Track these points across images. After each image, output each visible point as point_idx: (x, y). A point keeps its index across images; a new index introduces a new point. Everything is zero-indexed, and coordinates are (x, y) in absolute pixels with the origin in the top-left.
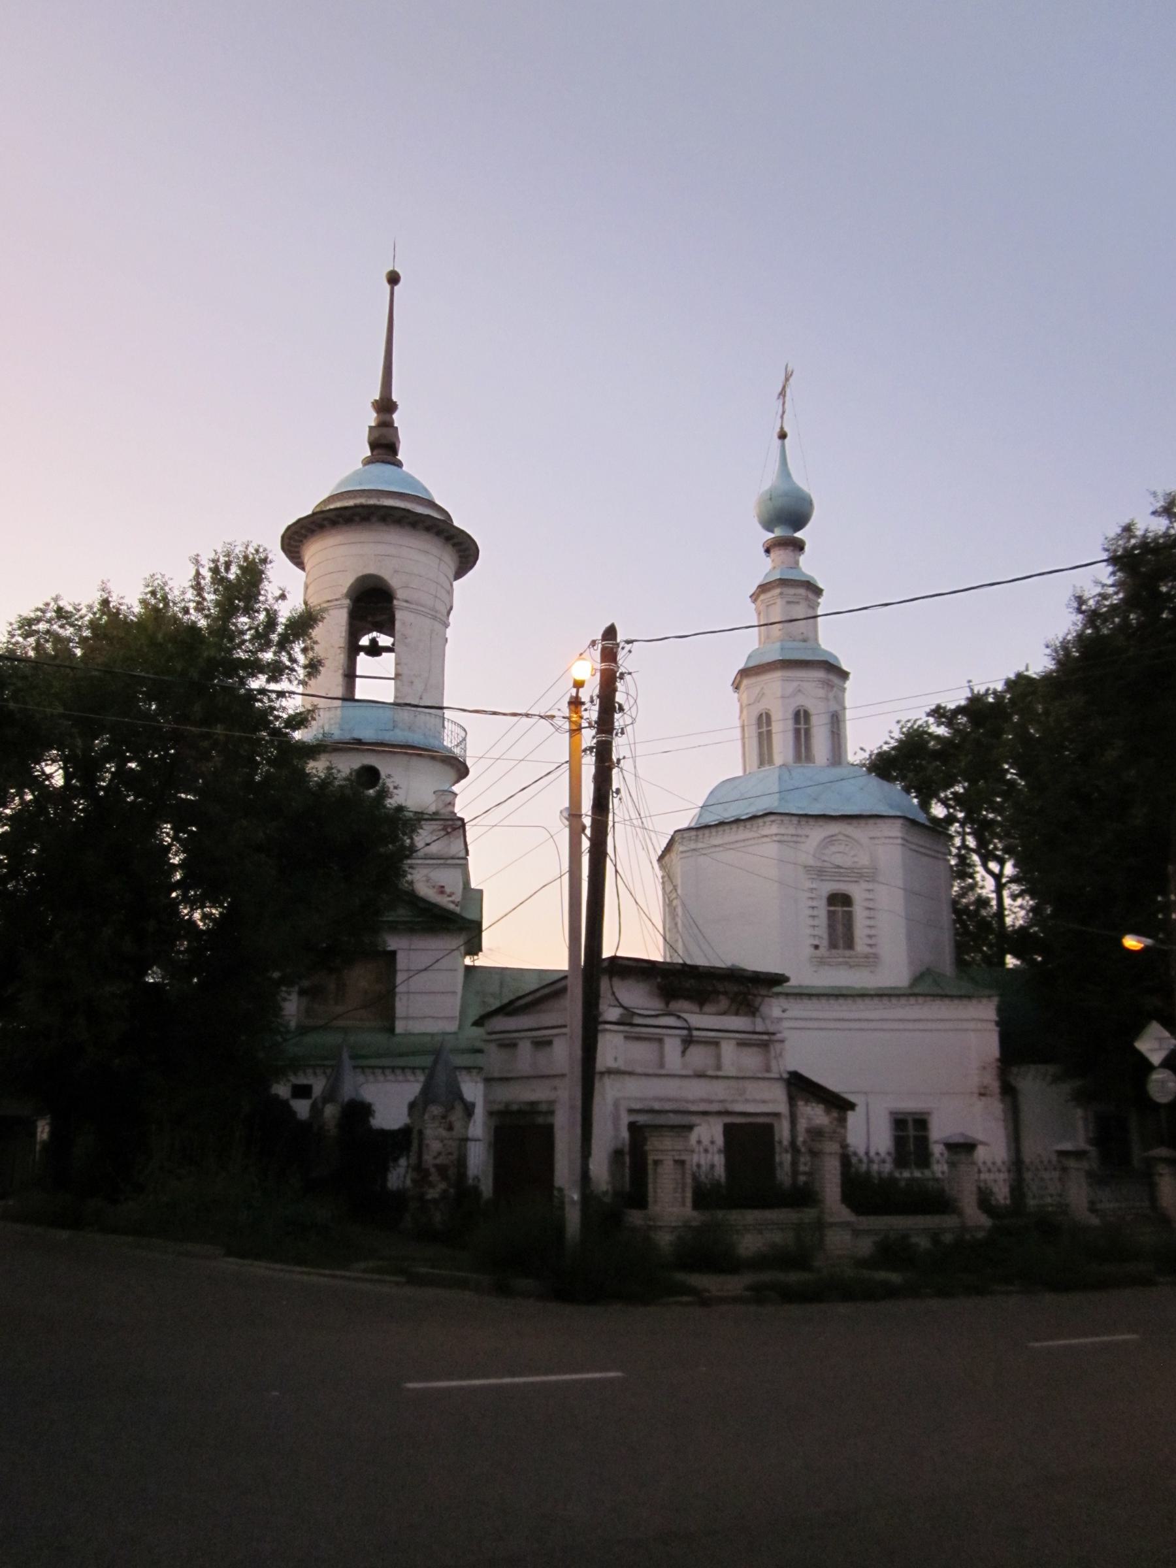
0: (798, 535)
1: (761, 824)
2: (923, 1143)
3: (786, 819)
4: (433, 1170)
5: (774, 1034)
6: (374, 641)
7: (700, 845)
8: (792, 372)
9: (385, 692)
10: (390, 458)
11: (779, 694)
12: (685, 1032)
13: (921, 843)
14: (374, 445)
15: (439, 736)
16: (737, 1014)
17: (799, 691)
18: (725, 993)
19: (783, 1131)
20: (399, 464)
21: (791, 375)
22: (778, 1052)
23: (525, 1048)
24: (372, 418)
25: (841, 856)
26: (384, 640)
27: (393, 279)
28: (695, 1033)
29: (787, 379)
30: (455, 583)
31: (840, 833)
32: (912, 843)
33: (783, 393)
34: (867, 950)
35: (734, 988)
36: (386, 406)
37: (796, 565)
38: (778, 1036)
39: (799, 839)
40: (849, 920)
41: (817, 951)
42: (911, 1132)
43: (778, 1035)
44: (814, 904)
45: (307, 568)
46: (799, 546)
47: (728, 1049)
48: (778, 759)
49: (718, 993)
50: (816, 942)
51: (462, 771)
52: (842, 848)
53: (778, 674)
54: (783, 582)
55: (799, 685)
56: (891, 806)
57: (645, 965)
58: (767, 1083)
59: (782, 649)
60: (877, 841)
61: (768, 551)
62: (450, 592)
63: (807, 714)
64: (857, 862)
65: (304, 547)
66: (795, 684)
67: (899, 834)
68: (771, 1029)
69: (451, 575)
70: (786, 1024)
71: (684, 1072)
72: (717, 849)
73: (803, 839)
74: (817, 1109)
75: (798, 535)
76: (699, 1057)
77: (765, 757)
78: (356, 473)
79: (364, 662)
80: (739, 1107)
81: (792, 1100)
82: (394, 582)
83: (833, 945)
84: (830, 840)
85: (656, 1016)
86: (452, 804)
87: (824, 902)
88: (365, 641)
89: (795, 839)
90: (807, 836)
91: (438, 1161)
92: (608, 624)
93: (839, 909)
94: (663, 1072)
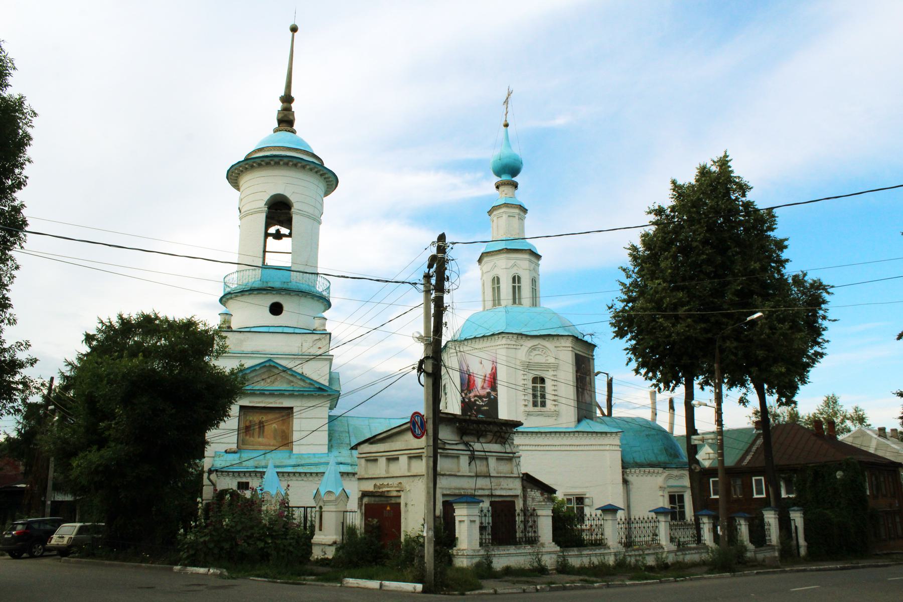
0: (514, 179)
1: (497, 338)
3: (510, 336)
5: (515, 453)
6: (278, 231)
8: (512, 91)
9: (285, 261)
10: (289, 128)
12: (469, 453)
13: (581, 350)
14: (280, 121)
15: (314, 287)
16: (496, 443)
18: (491, 431)
19: (519, 505)
20: (294, 132)
21: (512, 93)
22: (517, 462)
23: (382, 462)
24: (279, 105)
25: (538, 358)
26: (285, 231)
27: (294, 29)
29: (509, 95)
30: (325, 199)
31: (539, 344)
32: (576, 350)
33: (506, 102)
34: (553, 408)
35: (496, 429)
36: (287, 99)
37: (513, 197)
38: (517, 454)
39: (517, 347)
43: (517, 454)
45: (241, 190)
46: (515, 185)
47: (492, 462)
48: (503, 303)
49: (486, 431)
50: (526, 403)
51: (328, 305)
53: (503, 256)
54: (506, 205)
55: (515, 262)
57: (450, 416)
58: (512, 479)
60: (558, 349)
61: (497, 187)
62: (322, 205)
63: (519, 278)
64: (548, 360)
65: (241, 177)
66: (513, 262)
67: (570, 345)
68: (514, 450)
69: (322, 194)
70: (521, 448)
71: (469, 474)
73: (519, 347)
74: (537, 493)
75: (514, 179)
76: (480, 467)
77: (497, 301)
78: (270, 135)
79: (271, 242)
80: (498, 493)
81: (524, 489)
82: (292, 198)
83: (535, 404)
84: (534, 348)
85: (456, 444)
86: (324, 325)
88: (272, 230)
89: (515, 347)
90: (521, 346)
92: (441, 233)
93: (539, 385)
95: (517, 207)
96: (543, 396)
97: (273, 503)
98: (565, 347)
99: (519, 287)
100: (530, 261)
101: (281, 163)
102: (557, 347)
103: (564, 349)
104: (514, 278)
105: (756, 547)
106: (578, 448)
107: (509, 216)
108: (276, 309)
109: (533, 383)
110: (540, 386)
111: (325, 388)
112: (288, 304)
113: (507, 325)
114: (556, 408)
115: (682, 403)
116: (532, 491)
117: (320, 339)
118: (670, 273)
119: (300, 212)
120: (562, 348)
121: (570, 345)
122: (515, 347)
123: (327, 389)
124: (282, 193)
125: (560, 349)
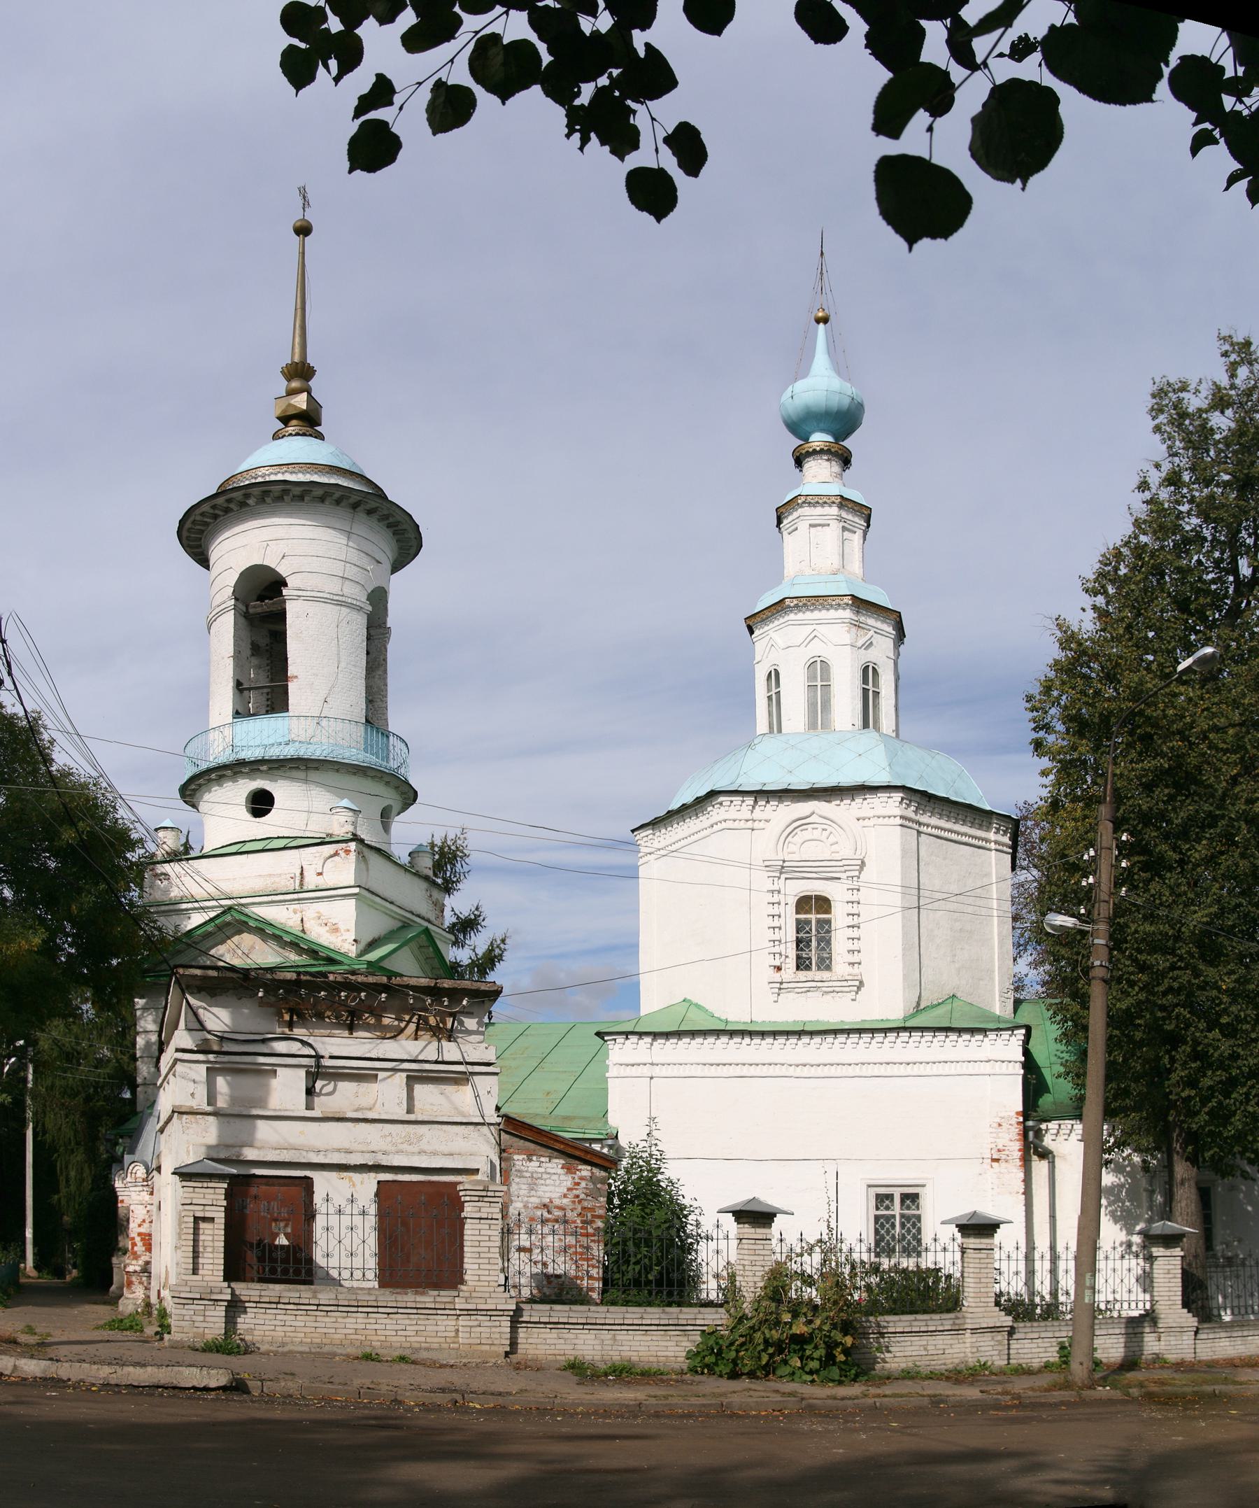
2: (913, 1223)
4: (138, 1239)
12: (311, 1062)
25: (808, 847)
28: (326, 1062)
39: (756, 825)
40: (825, 925)
41: (778, 974)
42: (897, 1210)
52: (816, 834)
60: (866, 822)
73: (762, 825)
84: (801, 823)
87: (792, 908)
89: (750, 824)
91: (142, 1230)
94: (412, 1117)
96: (825, 942)
97: (844, 1250)
99: (876, 694)
101: (251, 502)
105: (1199, 1322)
106: (909, 1070)
107: (811, 526)
108: (261, 804)
111: (338, 958)
112: (281, 790)
114: (856, 970)
115: (300, 855)
116: (531, 1160)
117: (336, 854)
119: (300, 593)
121: (898, 812)
122: (750, 824)
123: (342, 959)
124: (259, 562)
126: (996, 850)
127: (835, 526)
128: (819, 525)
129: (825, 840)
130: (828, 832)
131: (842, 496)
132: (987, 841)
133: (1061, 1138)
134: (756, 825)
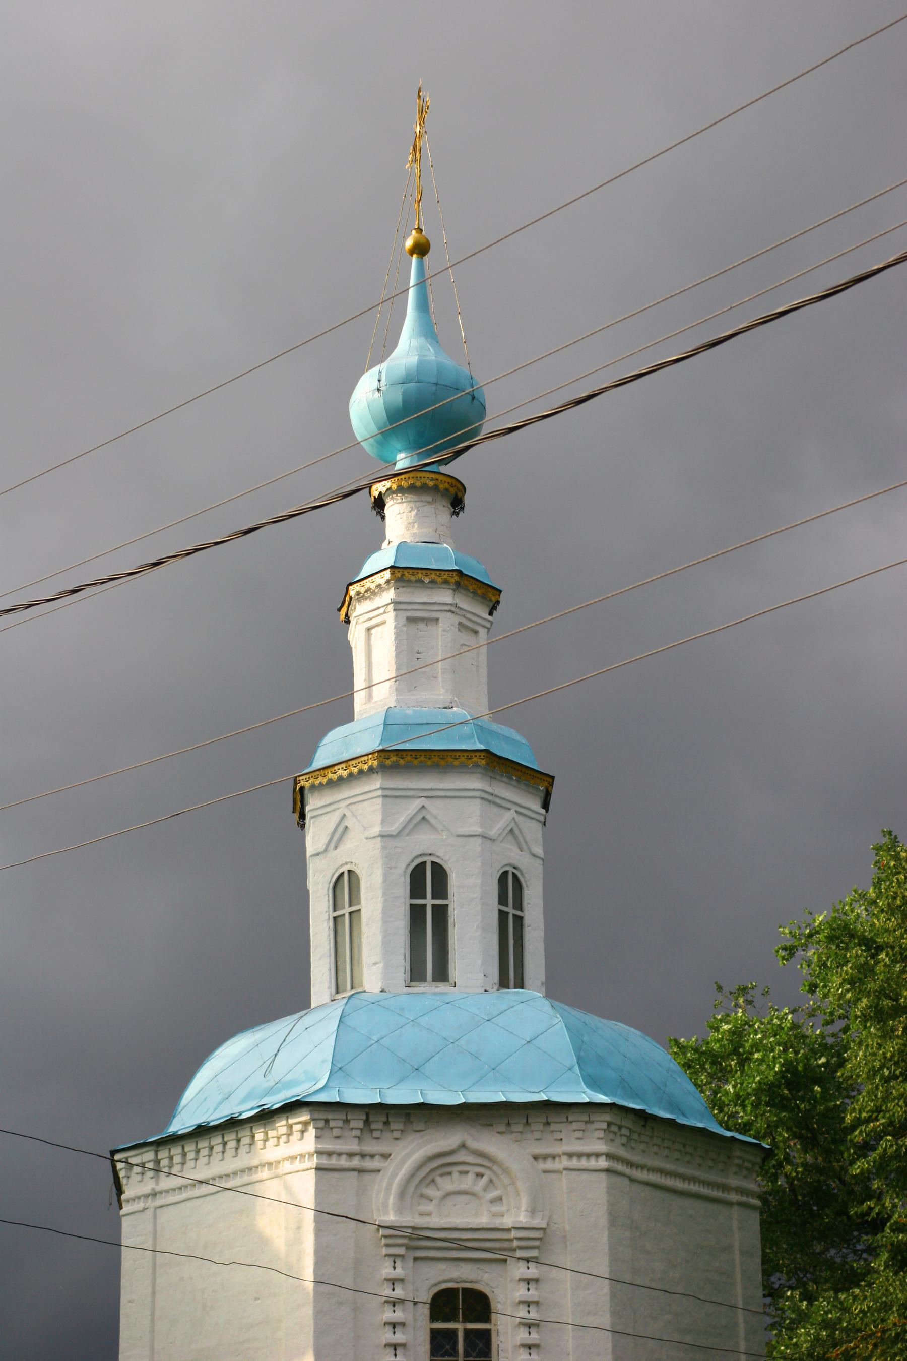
7: (166, 1183)
11: (376, 830)
13: (658, 1163)
17: (422, 820)
31: (463, 1146)
32: (642, 1167)
39: (368, 1164)
44: (398, 1315)
52: (467, 1182)
56: (593, 1083)
59: (385, 725)
60: (549, 1165)
63: (440, 873)
72: (205, 1189)
87: (425, 1311)
89: (356, 1162)
93: (459, 1327)
95: (446, 582)
98: (580, 1155)
100: (490, 800)
102: (545, 1157)
103: (574, 1163)
104: (417, 875)
109: (434, 1318)
110: (467, 1332)
113: (338, 1070)
118: (839, 1101)
120: (565, 1162)
122: (356, 1162)
125: (557, 1165)
126: (740, 1204)
127: (448, 622)
128: (422, 619)
129: (481, 1193)
130: (485, 1179)
131: (459, 572)
132: (725, 1188)
133: (190, 1164)
134: (368, 1164)
